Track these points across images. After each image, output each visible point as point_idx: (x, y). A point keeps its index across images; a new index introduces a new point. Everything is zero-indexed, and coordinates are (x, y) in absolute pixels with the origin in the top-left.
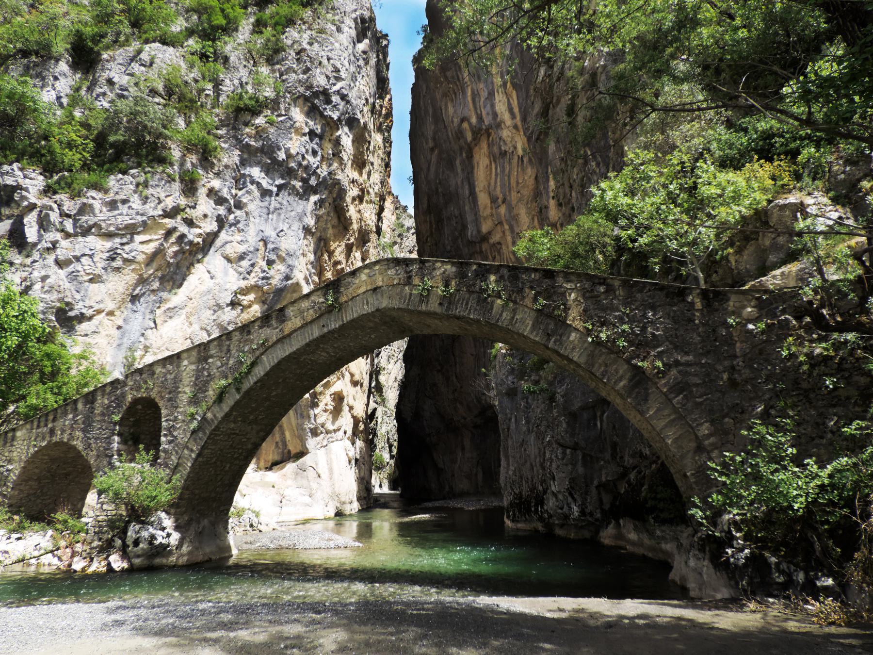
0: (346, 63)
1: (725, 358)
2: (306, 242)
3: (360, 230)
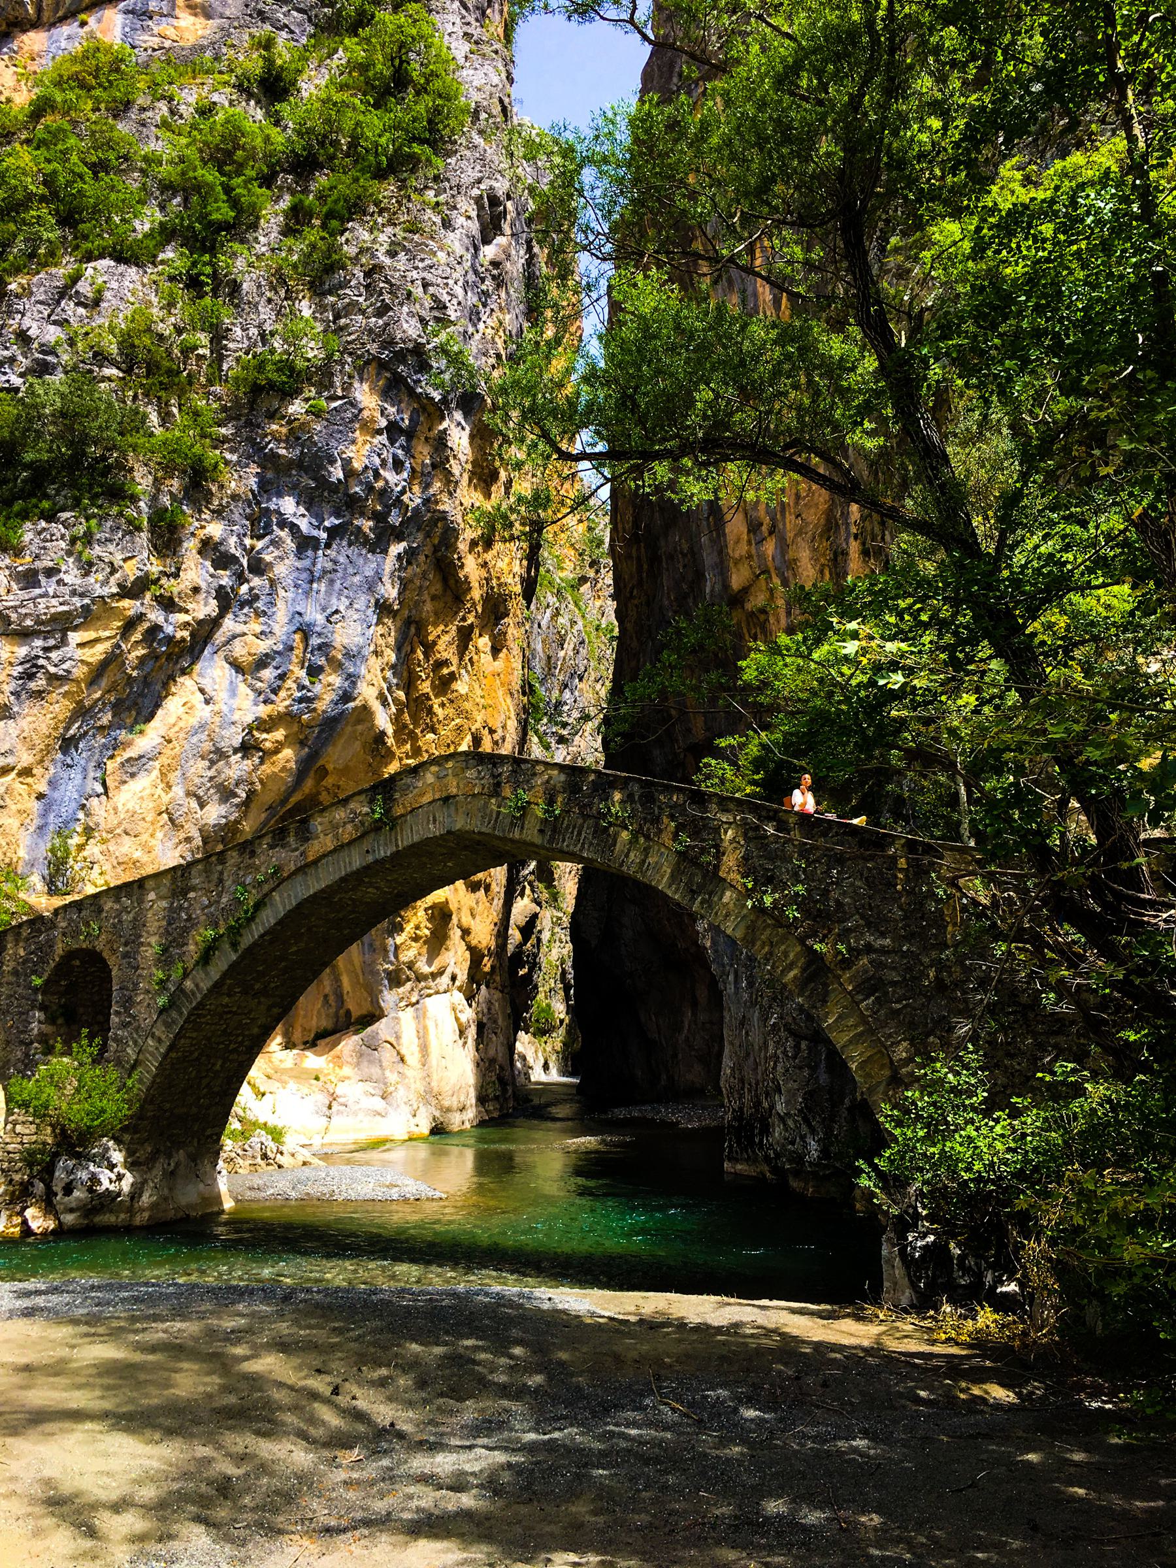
0: (459, 291)
1: (933, 947)
2: (381, 630)
3: (488, 599)
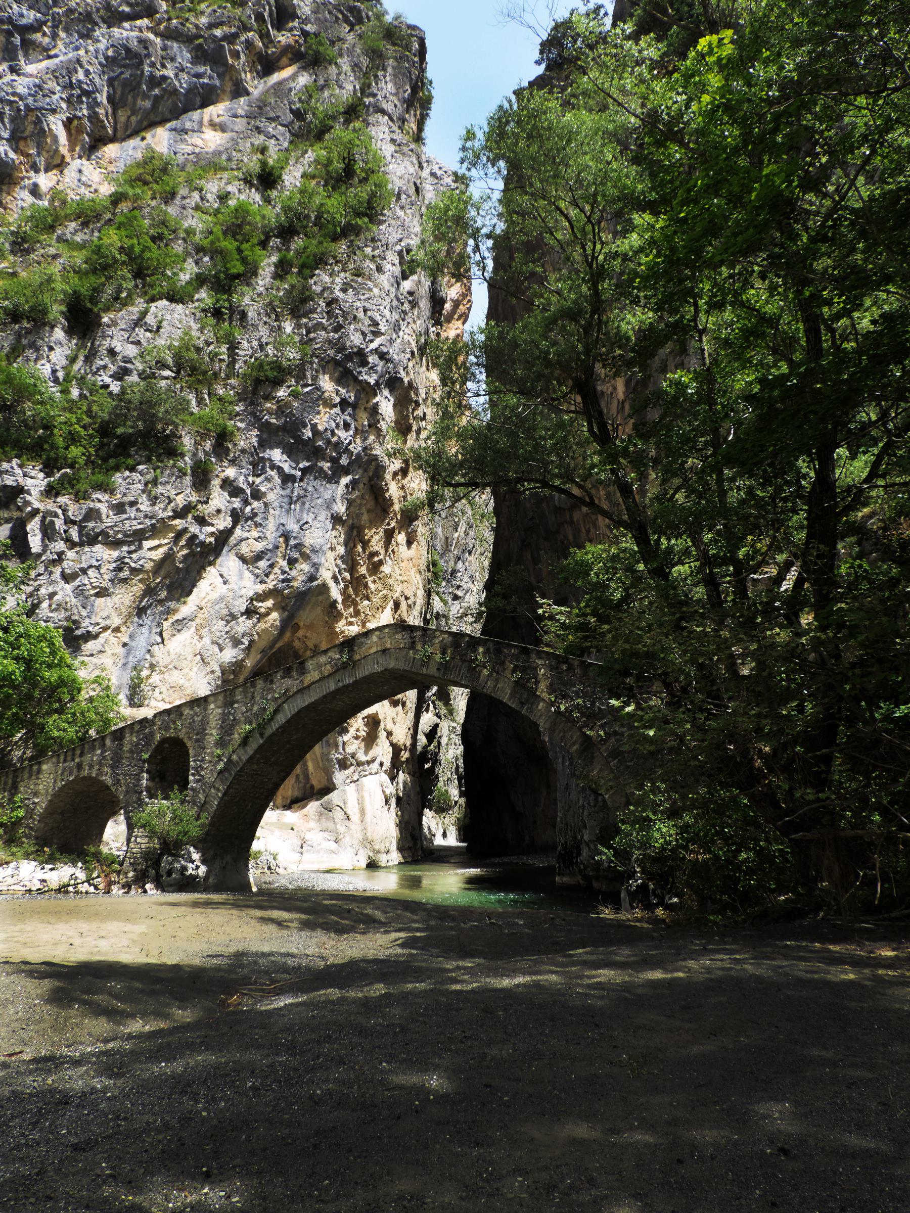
0: (387, 312)
2: (334, 533)
